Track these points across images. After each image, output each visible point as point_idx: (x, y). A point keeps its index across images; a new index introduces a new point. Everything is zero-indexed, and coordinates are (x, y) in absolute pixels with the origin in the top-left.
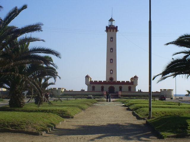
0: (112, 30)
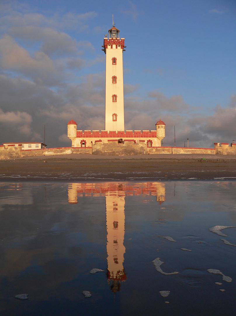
0: (114, 46)
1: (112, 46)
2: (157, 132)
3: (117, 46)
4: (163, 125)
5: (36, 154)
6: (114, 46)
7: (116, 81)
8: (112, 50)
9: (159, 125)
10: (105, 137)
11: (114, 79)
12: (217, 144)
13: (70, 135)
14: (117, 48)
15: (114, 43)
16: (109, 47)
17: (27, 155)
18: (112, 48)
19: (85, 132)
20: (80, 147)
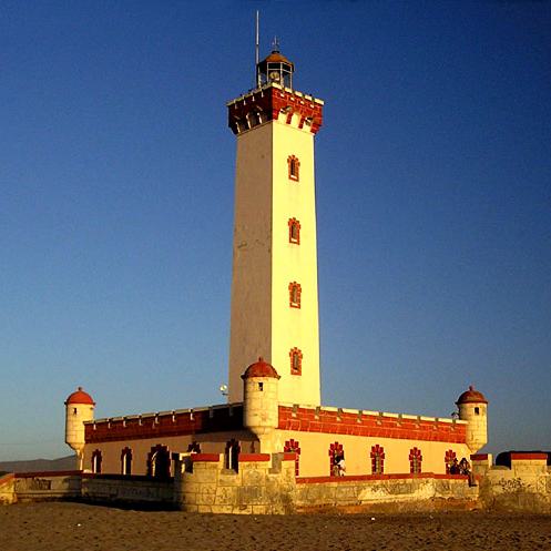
0: (296, 118)
1: (290, 116)
2: (471, 428)
3: (302, 120)
4: (485, 405)
5: (340, 496)
6: (296, 118)
7: (298, 238)
8: (287, 127)
9: (479, 405)
10: (453, 442)
11: (294, 227)
12: (486, 457)
13: (264, 419)
14: (301, 127)
15: (297, 109)
16: (282, 117)
17: (314, 501)
18: (289, 122)
19: (405, 420)
20: (370, 473)
